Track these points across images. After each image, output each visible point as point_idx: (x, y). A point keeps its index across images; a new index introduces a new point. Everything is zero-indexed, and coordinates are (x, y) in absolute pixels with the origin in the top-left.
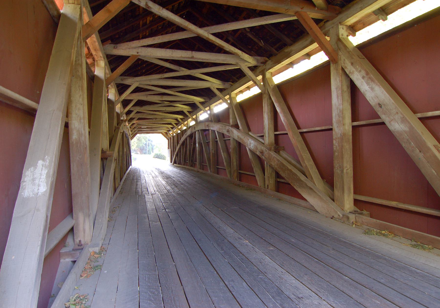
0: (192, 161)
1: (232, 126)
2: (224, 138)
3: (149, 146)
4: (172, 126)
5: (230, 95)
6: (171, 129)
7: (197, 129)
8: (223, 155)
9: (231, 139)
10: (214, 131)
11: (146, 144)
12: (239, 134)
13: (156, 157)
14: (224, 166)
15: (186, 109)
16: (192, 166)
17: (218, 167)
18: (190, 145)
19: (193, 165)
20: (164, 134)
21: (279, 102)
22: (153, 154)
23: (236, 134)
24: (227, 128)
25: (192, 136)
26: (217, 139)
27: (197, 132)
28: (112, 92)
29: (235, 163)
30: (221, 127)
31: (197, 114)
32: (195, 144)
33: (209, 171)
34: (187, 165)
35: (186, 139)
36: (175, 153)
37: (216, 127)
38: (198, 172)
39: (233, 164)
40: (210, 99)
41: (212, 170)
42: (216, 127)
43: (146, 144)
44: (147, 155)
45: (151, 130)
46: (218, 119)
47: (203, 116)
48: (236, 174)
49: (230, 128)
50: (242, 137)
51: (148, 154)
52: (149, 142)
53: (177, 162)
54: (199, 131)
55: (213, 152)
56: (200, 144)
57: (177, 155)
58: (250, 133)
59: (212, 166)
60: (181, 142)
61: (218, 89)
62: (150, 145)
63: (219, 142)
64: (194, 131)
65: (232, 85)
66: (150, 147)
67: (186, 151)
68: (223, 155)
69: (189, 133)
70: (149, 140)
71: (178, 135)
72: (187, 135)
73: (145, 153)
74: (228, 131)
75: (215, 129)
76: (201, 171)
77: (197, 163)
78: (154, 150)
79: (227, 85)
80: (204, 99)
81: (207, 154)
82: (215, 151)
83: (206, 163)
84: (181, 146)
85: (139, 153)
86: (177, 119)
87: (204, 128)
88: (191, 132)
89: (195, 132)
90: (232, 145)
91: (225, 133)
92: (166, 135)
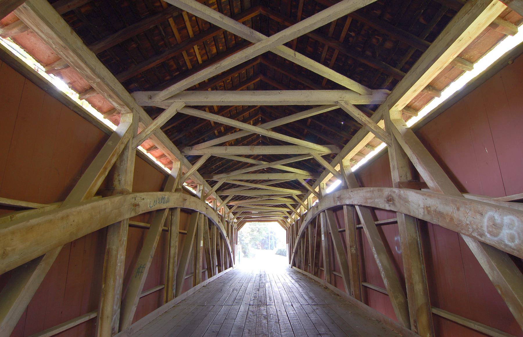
0: (316, 265)
1: (401, 185)
2: (376, 219)
3: (271, 239)
4: (288, 210)
5: (386, 117)
6: (288, 215)
7: (321, 208)
8: (379, 260)
9: (400, 219)
10: (353, 206)
11: (268, 238)
12: (434, 203)
13: (279, 254)
14: (382, 285)
15: (301, 175)
16: (316, 274)
17: (365, 284)
18: (313, 237)
19: (318, 273)
20: (281, 222)
21: (426, 165)
22: (276, 250)
23: (416, 202)
24: (387, 191)
25: (314, 222)
26: (359, 222)
27: (321, 214)
28: (127, 120)
29: (418, 286)
30: (369, 195)
31: (321, 184)
32: (319, 234)
33: (347, 291)
34: (310, 272)
35: (307, 228)
36: (294, 251)
37: (358, 197)
38: (326, 288)
39: (412, 289)
40: (341, 148)
41: (352, 289)
42: (358, 197)
43: (268, 238)
44: (269, 251)
45: (264, 218)
46: (359, 180)
47: (331, 185)
48: (424, 319)
49: (396, 190)
50: (448, 209)
51: (271, 249)
52: (272, 234)
53: (297, 265)
54: (324, 211)
55: (353, 251)
56: (328, 234)
57: (296, 253)
58: (466, 196)
59: (352, 282)
60: (300, 233)
61: (359, 107)
62: (273, 238)
63: (365, 230)
64: (316, 212)
65: (388, 95)
66: (273, 241)
67: (307, 248)
68: (379, 260)
69: (309, 217)
70: (271, 232)
71: (297, 222)
72: (308, 221)
73: (267, 249)
74: (390, 200)
75: (355, 203)
76: (331, 287)
77: (325, 269)
78: (277, 245)
79: (378, 96)
80: (331, 149)
81: (340, 254)
82: (356, 250)
83: (340, 273)
84: (300, 238)
85: (260, 247)
86: (291, 197)
87: (333, 205)
88: (313, 214)
89: (319, 215)
90: (404, 237)
91: (381, 204)
92: (283, 223)
